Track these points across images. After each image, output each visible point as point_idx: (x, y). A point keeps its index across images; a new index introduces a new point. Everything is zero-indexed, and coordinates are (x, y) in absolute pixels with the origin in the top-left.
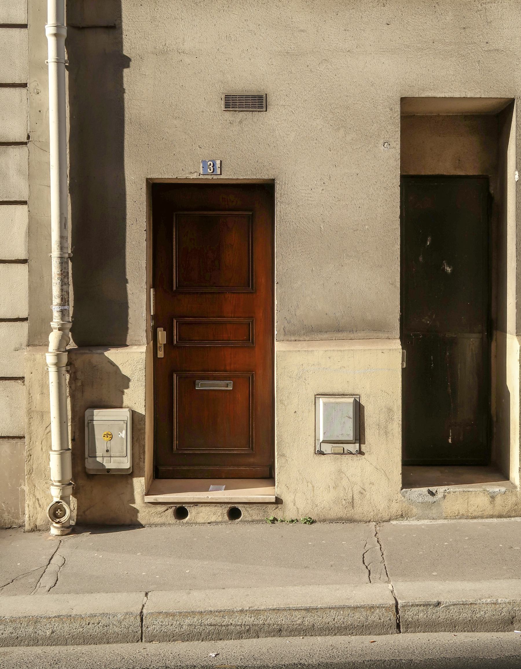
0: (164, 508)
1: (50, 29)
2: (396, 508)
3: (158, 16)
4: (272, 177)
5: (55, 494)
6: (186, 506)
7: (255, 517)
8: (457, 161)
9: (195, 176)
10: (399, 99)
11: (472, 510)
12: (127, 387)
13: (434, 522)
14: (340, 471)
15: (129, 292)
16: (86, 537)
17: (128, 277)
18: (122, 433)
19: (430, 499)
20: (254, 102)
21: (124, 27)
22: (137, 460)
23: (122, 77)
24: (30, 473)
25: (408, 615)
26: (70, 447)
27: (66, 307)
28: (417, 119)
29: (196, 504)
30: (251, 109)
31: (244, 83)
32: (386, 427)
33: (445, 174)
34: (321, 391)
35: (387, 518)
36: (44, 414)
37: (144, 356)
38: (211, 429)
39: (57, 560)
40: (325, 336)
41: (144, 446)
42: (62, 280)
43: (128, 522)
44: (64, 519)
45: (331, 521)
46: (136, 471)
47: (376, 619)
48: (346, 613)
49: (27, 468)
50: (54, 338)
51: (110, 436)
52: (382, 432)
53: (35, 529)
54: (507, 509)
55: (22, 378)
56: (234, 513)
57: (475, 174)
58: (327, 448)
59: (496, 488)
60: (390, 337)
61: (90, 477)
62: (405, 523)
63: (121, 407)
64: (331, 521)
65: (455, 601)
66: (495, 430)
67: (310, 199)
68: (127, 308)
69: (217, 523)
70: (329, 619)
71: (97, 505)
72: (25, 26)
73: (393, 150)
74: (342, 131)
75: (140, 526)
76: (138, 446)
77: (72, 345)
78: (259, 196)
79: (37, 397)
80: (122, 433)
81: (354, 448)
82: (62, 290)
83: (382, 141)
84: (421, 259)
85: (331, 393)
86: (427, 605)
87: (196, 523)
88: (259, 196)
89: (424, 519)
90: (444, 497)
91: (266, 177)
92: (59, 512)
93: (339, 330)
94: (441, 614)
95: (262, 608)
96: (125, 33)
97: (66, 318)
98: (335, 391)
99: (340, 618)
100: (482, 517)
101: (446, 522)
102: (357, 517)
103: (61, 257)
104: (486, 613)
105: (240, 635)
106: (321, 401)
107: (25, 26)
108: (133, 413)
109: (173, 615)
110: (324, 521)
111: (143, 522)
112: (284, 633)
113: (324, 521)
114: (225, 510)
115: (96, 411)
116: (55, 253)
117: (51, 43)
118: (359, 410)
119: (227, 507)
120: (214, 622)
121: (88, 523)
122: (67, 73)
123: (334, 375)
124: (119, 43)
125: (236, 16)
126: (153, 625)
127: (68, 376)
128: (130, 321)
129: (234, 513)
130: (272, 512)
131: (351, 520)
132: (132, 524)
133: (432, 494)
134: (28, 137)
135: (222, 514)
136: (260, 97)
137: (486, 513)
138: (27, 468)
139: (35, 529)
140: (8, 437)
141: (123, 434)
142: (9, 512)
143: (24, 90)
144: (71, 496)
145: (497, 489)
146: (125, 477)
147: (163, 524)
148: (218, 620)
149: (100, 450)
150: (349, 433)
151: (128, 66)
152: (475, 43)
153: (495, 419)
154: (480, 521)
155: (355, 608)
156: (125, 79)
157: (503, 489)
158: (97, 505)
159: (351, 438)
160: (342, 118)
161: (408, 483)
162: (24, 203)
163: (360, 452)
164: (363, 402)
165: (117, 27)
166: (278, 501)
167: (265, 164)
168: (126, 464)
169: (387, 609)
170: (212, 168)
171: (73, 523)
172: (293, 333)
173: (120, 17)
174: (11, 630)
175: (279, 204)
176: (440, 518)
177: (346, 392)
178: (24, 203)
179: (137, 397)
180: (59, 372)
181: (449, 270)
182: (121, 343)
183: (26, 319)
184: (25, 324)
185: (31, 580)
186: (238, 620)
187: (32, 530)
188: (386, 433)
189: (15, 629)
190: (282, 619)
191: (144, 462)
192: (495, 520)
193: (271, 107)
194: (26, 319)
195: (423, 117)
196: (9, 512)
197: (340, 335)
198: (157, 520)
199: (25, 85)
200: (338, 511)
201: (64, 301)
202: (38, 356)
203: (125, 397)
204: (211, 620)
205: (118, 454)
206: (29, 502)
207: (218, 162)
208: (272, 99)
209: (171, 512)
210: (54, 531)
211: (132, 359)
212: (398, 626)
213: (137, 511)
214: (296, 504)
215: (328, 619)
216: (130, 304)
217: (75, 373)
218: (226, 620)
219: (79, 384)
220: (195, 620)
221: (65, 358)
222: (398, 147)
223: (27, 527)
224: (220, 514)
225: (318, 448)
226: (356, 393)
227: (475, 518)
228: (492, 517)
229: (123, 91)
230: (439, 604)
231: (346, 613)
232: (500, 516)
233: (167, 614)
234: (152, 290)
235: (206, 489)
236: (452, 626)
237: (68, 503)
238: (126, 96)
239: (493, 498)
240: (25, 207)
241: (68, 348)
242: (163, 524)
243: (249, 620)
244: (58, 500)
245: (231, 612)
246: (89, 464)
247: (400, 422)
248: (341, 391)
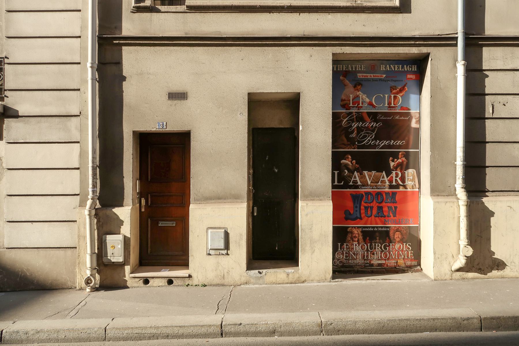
0: (138, 279)
1: (89, 65)
2: (243, 280)
5: (88, 273)
6: (149, 279)
7: (179, 284)
9: (154, 129)
11: (279, 280)
12: (123, 225)
13: (261, 286)
14: (218, 263)
15: (125, 182)
16: (102, 293)
17: (124, 175)
19: (259, 275)
20: (181, 96)
21: (124, 63)
22: (126, 258)
23: (122, 85)
24: (79, 264)
25: (226, 329)
26: (96, 251)
27: (95, 189)
28: (256, 103)
29: (153, 278)
31: (176, 88)
32: (239, 243)
34: (209, 226)
35: (239, 284)
36: (85, 237)
37: (130, 211)
38: (163, 244)
39: (84, 303)
40: (213, 201)
42: (93, 177)
43: (122, 286)
44: (91, 285)
45: (214, 285)
46: (126, 263)
47: (212, 331)
48: (198, 328)
49: (77, 262)
50: (89, 203)
51: (114, 247)
53: (81, 289)
54: (294, 280)
55: (76, 221)
56: (170, 282)
58: (212, 252)
59: (290, 270)
61: (106, 265)
62: (247, 286)
63: (120, 234)
64: (214, 285)
65: (248, 323)
68: (124, 189)
69: (162, 286)
70: (191, 331)
71: (108, 277)
72: (79, 63)
75: (128, 287)
77: (98, 206)
78: (184, 137)
79: (82, 229)
81: (225, 252)
82: (93, 181)
83: (239, 113)
84: (264, 166)
86: (235, 325)
87: (153, 286)
88: (184, 137)
89: (256, 284)
90: (266, 274)
91: (187, 130)
92: (89, 281)
93: (219, 198)
94: (241, 329)
95: (160, 326)
96: (124, 65)
97: (95, 194)
99: (196, 331)
100: (283, 284)
101: (266, 286)
102: (226, 284)
103: (93, 167)
104: (262, 328)
105: (149, 338)
106: (210, 231)
107: (79, 63)
108: (125, 237)
109: (120, 329)
110: (211, 285)
111: (129, 286)
112: (170, 337)
113: (211, 285)
114: (166, 280)
115: (107, 236)
116: (90, 165)
117: (90, 70)
118: (227, 235)
120: (138, 332)
121: (106, 286)
122: (97, 84)
123: (216, 220)
124: (121, 70)
126: (110, 334)
127: (96, 220)
128: (125, 195)
129: (170, 282)
130: (187, 282)
131: (223, 285)
132: (124, 286)
133: (260, 273)
134: (80, 113)
135: (165, 282)
136: (184, 93)
137: (285, 282)
138: (77, 262)
139: (81, 289)
140: (71, 248)
141: (120, 247)
142: (70, 281)
143: (78, 92)
144: (97, 274)
145: (290, 271)
146: (121, 266)
147: (138, 287)
148: (140, 331)
149: (109, 254)
150: (222, 245)
151: (125, 81)
154: (282, 285)
155: (202, 326)
156: (124, 86)
157: (293, 271)
158: (108, 277)
159: (223, 248)
161: (250, 267)
162: (78, 142)
163: (227, 254)
164: (228, 232)
166: (190, 276)
168: (121, 259)
169: (217, 326)
171: (97, 286)
172: (198, 200)
173: (122, 58)
174: (47, 335)
176: (263, 284)
177: (221, 227)
178: (78, 142)
179: (126, 230)
180: (90, 218)
181: (276, 171)
182: (120, 204)
183: (79, 195)
184: (78, 197)
185: (67, 312)
186: (149, 331)
187: (80, 290)
188: (239, 245)
189: (48, 335)
190: (169, 331)
192: (289, 285)
194: (79, 195)
195: (263, 101)
196: (70, 281)
197: (220, 201)
198: (135, 285)
199: (79, 90)
200: (216, 281)
201: (94, 186)
202: (83, 211)
203: (121, 229)
204: (137, 331)
206: (78, 276)
207: (165, 123)
209: (142, 281)
210: (88, 290)
211: (125, 213)
212: (222, 334)
213: (127, 281)
214: (198, 278)
215: (189, 331)
216: (125, 188)
217: (99, 219)
218: (143, 332)
219: (101, 223)
220: (130, 331)
221: (93, 212)
222: (247, 115)
223: (77, 288)
224: (164, 282)
225: (208, 252)
227: (280, 284)
228: (287, 283)
229: (123, 92)
230: (241, 324)
231: (198, 328)
232: (291, 283)
233: (117, 329)
235: (159, 271)
236: (247, 334)
237: (95, 278)
238: (124, 94)
239: (288, 275)
240: (79, 144)
241: (96, 207)
242: (138, 287)
243: (154, 331)
244: (89, 276)
245: (146, 328)
246: (104, 260)
248: (219, 226)
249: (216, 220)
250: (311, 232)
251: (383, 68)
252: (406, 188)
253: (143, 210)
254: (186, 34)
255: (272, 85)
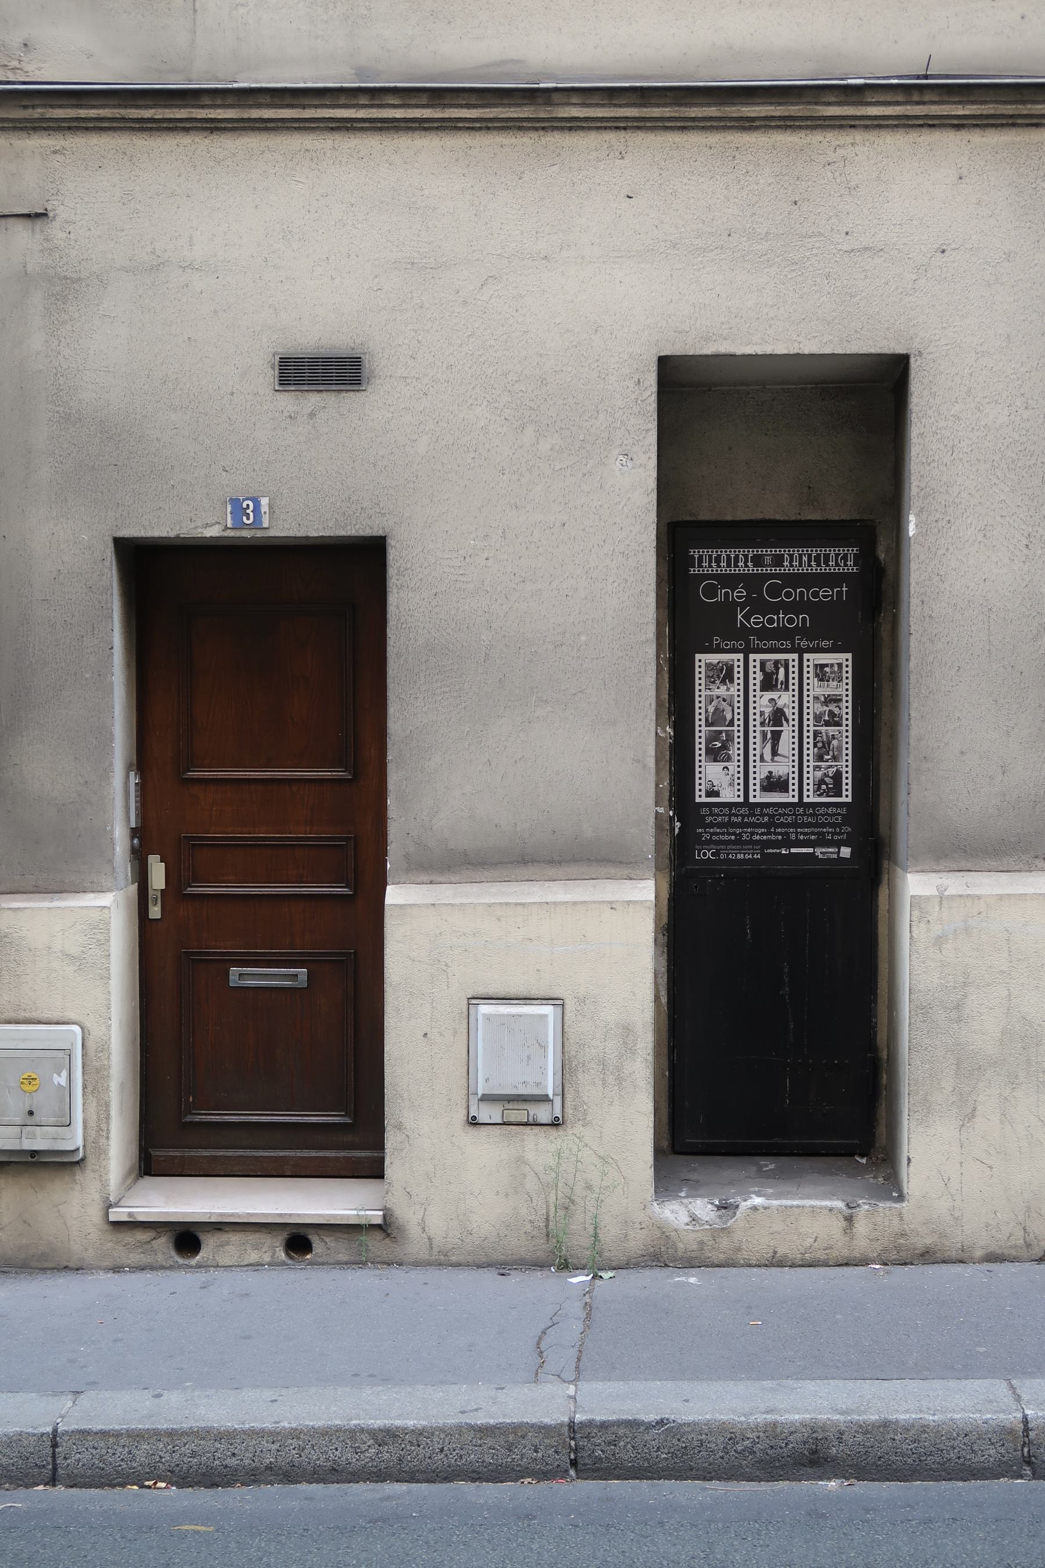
3: (138, 188)
4: (381, 533)
8: (806, 490)
10: (656, 359)
14: (520, 1160)
18: (59, 1075)
20: (324, 372)
22: (93, 1133)
28: (691, 393)
30: (334, 387)
31: (317, 334)
32: (619, 1069)
33: (778, 517)
34: (482, 991)
41: (107, 1105)
52: (611, 1079)
54: (878, 1247)
57: (844, 517)
60: (633, 876)
66: (884, 1080)
67: (461, 578)
73: (641, 470)
74: (530, 431)
76: (95, 1104)
80: (59, 1075)
85: (501, 995)
98: (512, 991)
119: (284, 1235)
123: (522, 971)
125: (301, 186)
152: (820, 234)
153: (884, 1055)
160: (531, 404)
165: (51, 214)
167: (365, 505)
170: (251, 515)
175: (395, 591)
177: (534, 993)
188: (620, 1080)
191: (108, 1138)
193: (378, 382)
205: (52, 1120)
208: (271, 375)
226: (555, 996)
234: (132, 774)
247: (651, 1058)
249: (522, 971)
250: (959, 1020)
251: (766, 819)
252: (78, 1149)
253: (155, 912)
254: (361, 72)
255: (776, 313)
